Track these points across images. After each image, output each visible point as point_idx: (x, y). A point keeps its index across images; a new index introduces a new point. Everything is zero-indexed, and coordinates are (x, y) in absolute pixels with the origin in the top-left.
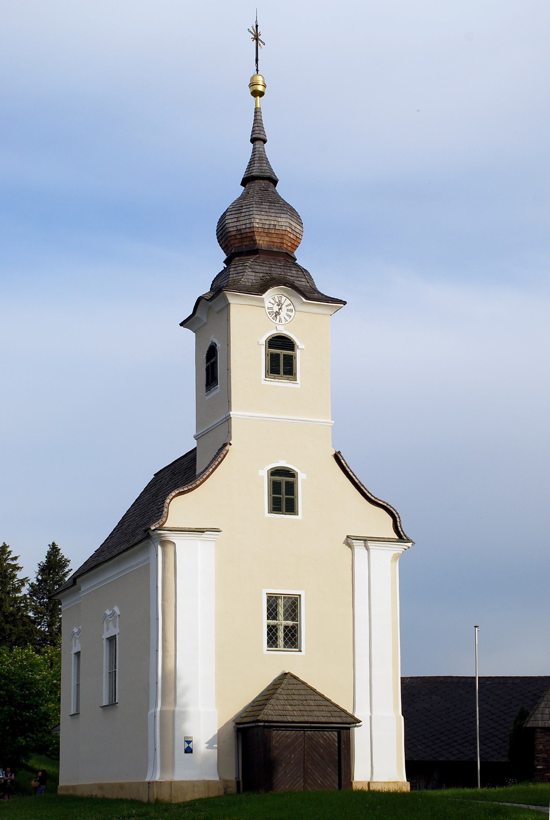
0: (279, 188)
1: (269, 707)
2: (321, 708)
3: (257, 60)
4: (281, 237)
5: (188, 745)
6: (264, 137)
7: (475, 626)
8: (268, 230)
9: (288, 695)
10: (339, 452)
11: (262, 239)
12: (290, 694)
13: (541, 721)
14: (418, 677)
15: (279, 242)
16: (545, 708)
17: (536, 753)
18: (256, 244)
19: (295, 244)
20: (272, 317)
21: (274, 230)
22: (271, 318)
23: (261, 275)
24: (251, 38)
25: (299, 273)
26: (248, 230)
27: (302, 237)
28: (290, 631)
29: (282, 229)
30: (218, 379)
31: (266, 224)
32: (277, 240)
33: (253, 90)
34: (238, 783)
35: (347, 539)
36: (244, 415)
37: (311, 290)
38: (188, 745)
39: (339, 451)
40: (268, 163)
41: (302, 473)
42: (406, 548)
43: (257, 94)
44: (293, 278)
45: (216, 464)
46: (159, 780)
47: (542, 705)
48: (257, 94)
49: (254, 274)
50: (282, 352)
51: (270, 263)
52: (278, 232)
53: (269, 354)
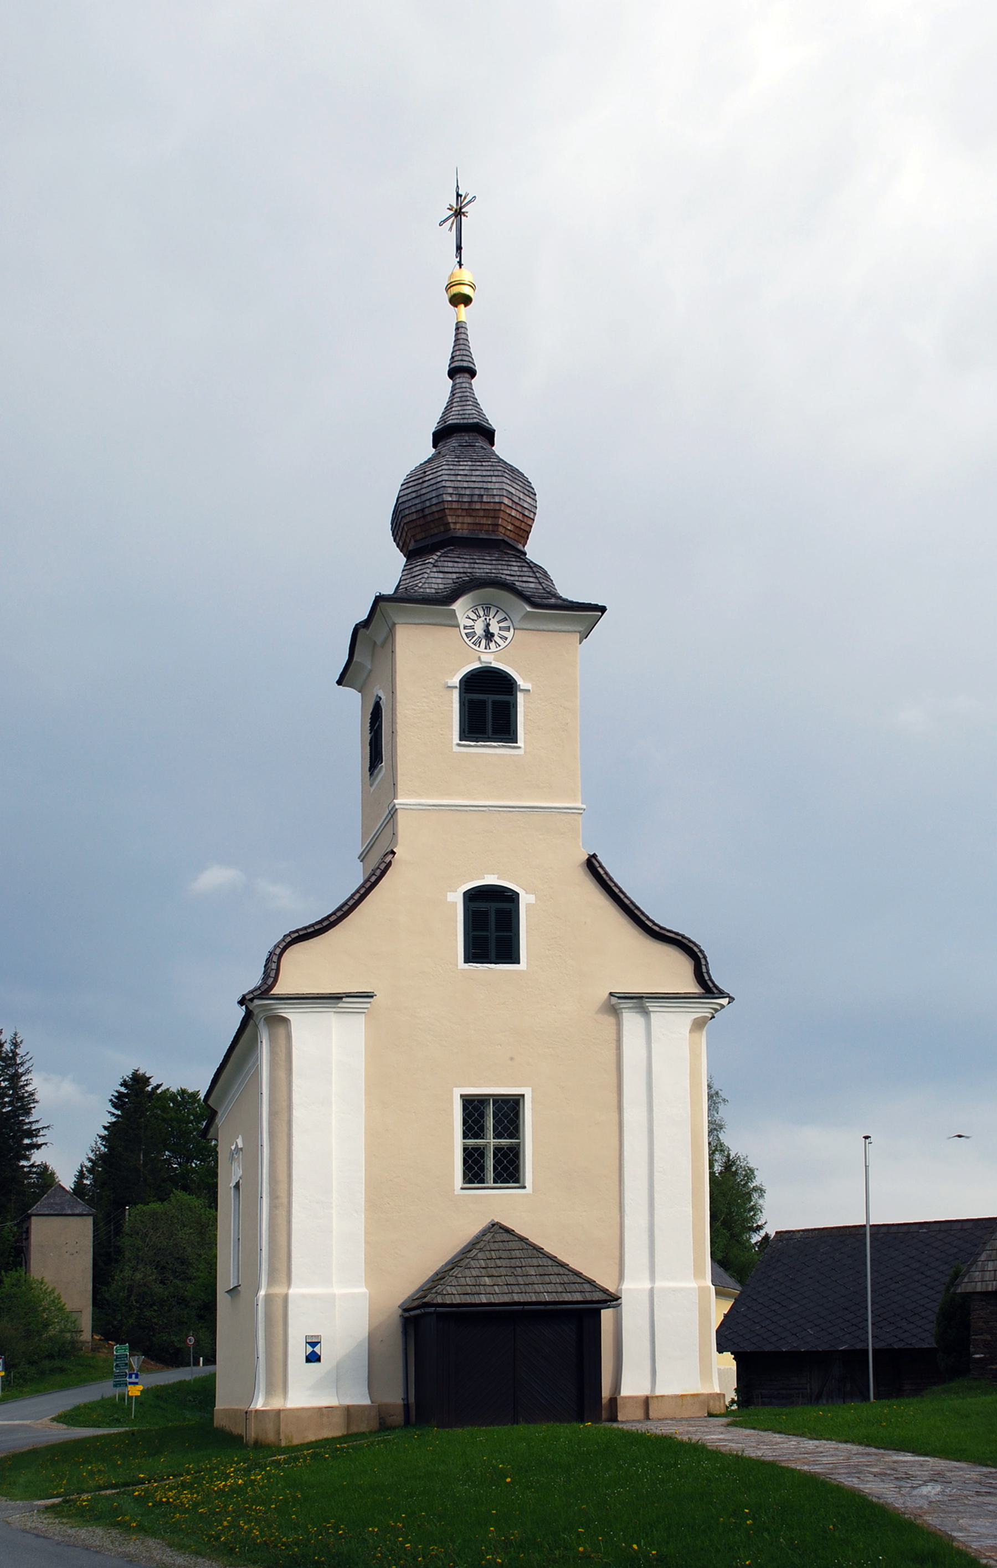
0: (501, 448)
1: (449, 1281)
2: (547, 1279)
3: (459, 248)
4: (492, 515)
5: (312, 1349)
6: (471, 365)
7: (864, 1137)
8: (469, 505)
9: (488, 1259)
10: (594, 856)
11: (460, 521)
12: (492, 1259)
13: (980, 1283)
14: (815, 1229)
15: (489, 523)
16: (988, 1261)
17: (972, 1334)
18: (450, 530)
19: (522, 527)
20: (472, 641)
21: (479, 504)
22: (470, 643)
23: (454, 576)
24: (450, 205)
25: (525, 569)
26: (434, 509)
27: (534, 517)
28: (505, 1155)
29: (494, 501)
30: (383, 753)
31: (465, 495)
32: (487, 520)
33: (452, 294)
34: (406, 1406)
35: (610, 999)
36: (419, 805)
37: (545, 595)
38: (312, 1349)
39: (595, 854)
40: (476, 404)
41: (527, 893)
42: (718, 1007)
43: (460, 300)
44: (512, 578)
45: (367, 887)
46: (262, 1407)
47: (983, 1257)
48: (460, 300)
49: (441, 575)
50: (490, 698)
51: (472, 557)
52: (487, 508)
53: (466, 702)
